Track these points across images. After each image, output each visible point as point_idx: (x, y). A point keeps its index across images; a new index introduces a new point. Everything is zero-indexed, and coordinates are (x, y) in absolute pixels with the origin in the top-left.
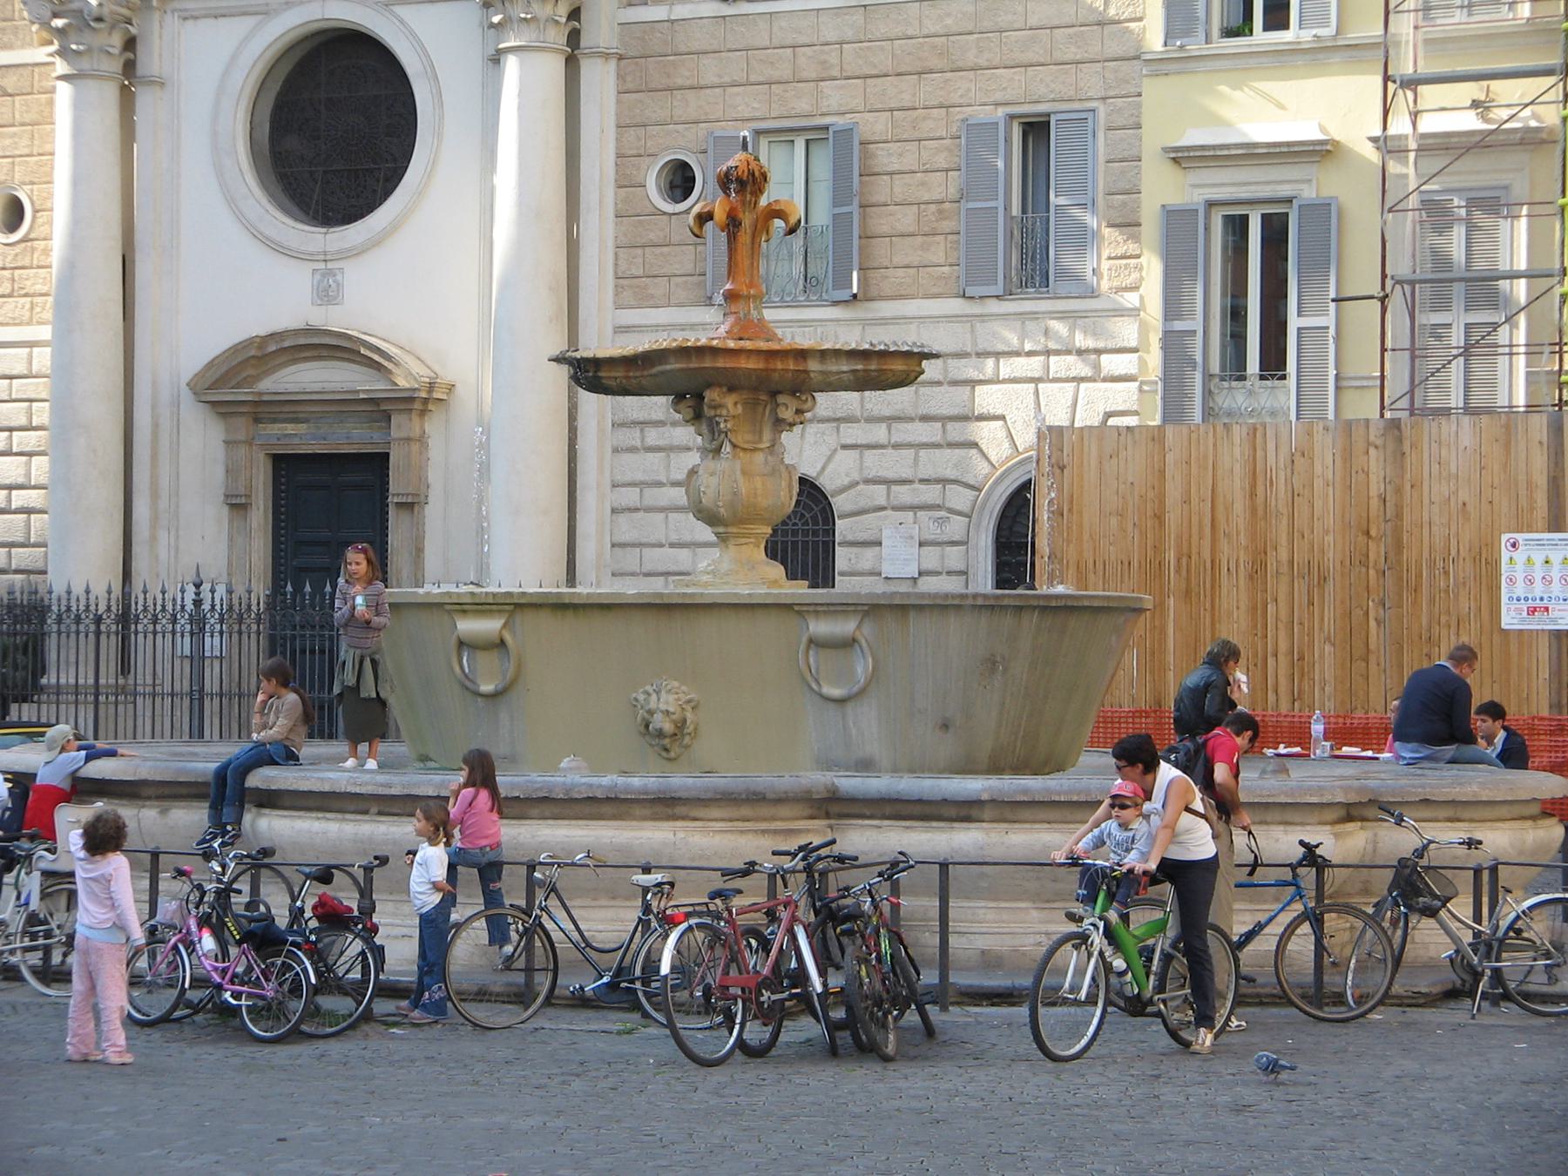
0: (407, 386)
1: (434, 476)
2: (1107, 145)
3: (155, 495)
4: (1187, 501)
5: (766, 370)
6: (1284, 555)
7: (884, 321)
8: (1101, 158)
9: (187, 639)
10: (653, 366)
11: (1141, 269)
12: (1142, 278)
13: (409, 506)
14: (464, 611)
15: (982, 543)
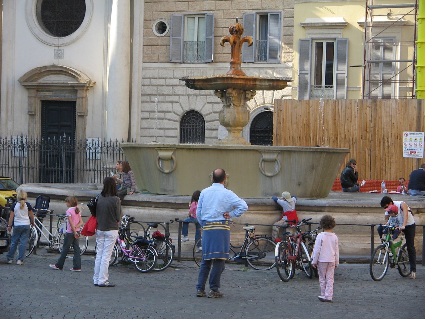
0: (83, 82)
1: (89, 108)
2: (284, 22)
3: (7, 111)
4: (316, 121)
5: (245, 84)
6: (343, 136)
7: (220, 68)
8: (282, 25)
9: (19, 152)
10: (212, 82)
11: (293, 56)
12: (293, 59)
13: (82, 116)
14: (161, 150)
15: (247, 130)
